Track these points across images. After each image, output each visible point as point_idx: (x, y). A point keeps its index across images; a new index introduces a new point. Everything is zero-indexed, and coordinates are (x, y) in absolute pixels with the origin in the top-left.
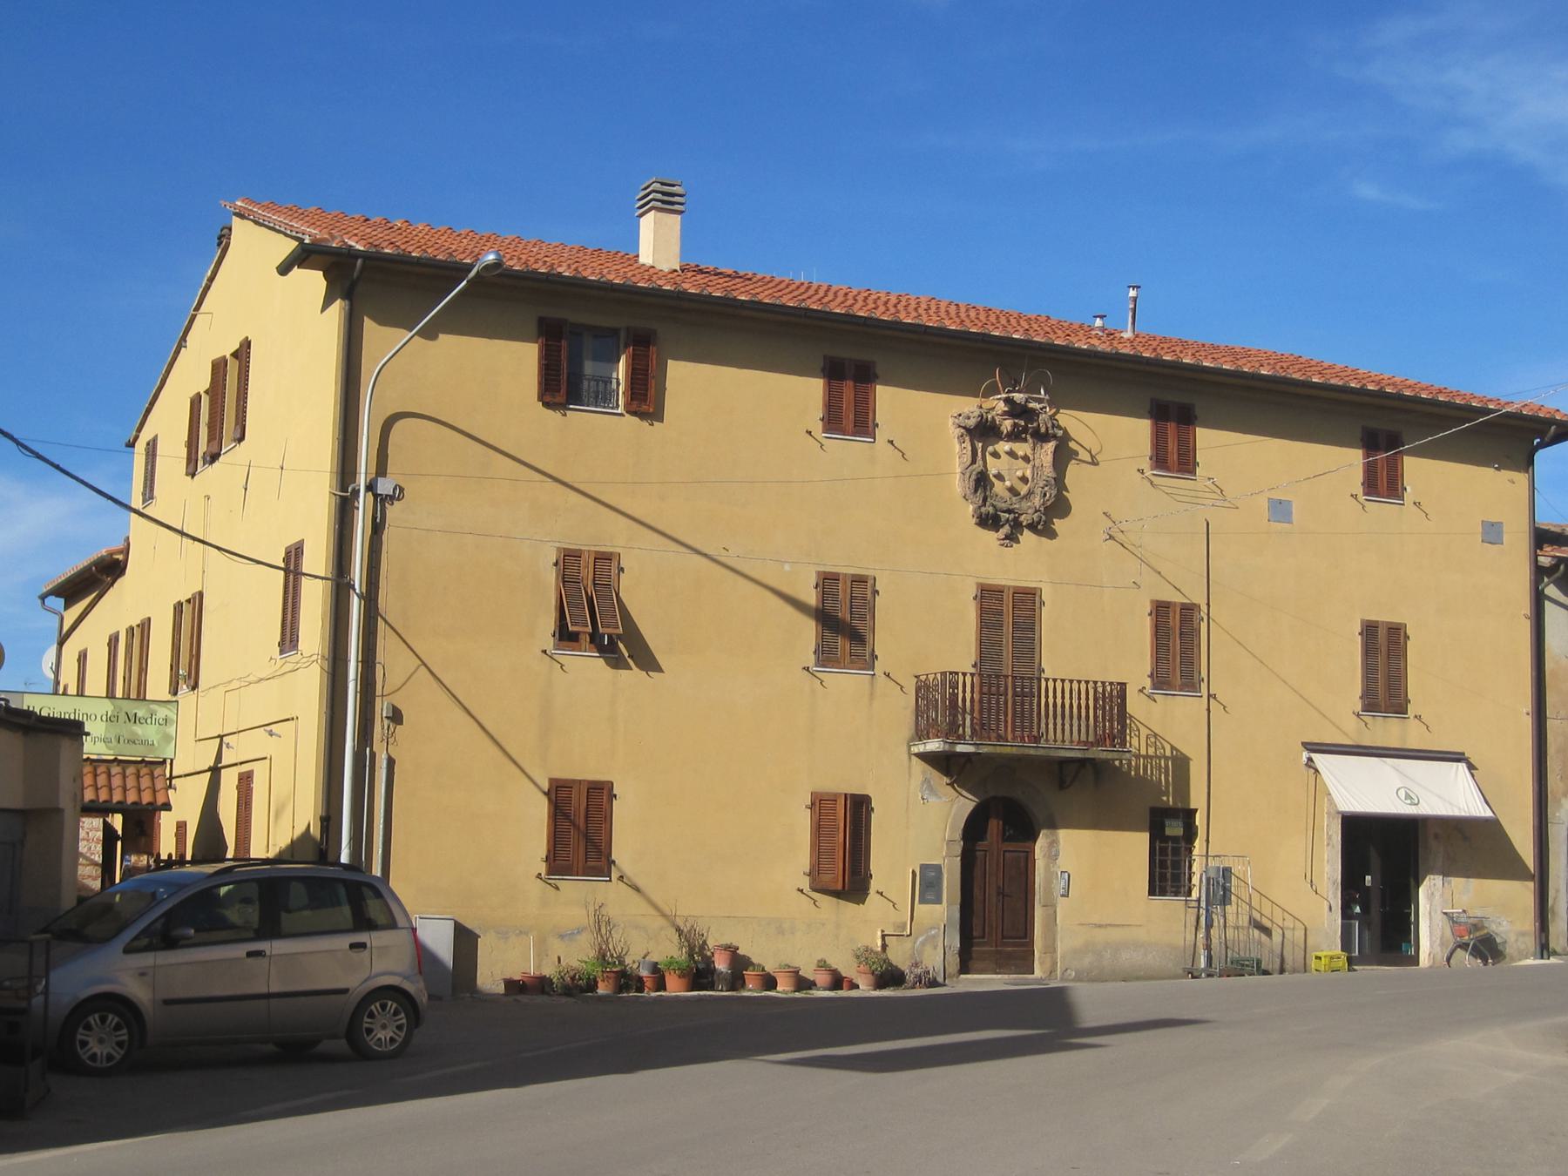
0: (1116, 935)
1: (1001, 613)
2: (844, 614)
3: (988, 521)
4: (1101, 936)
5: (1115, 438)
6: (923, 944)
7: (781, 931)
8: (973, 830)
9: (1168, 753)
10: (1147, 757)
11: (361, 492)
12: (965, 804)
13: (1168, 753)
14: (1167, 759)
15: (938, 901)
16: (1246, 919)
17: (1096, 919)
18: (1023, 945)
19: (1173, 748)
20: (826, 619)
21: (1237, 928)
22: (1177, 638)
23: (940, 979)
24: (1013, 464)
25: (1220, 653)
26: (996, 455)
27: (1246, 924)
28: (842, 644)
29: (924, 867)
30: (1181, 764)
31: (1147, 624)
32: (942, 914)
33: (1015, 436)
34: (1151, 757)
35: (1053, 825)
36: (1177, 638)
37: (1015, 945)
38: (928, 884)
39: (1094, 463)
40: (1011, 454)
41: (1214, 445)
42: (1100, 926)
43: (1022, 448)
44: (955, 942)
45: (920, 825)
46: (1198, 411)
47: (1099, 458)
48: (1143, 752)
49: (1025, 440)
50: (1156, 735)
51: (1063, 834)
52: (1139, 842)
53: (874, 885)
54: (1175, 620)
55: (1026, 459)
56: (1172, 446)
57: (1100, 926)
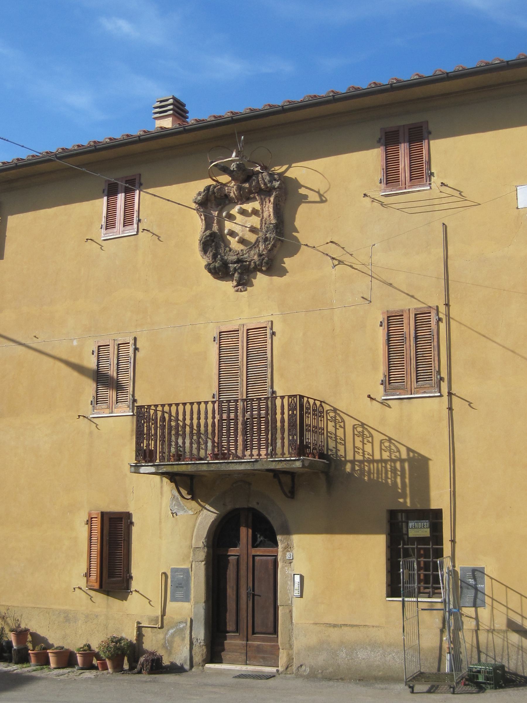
0: (350, 635)
1: (236, 349)
2: (112, 372)
3: (220, 271)
4: (335, 634)
5: (340, 181)
6: (173, 635)
7: (67, 619)
8: (220, 540)
9: (404, 456)
10: (382, 461)
11: (522, 656)
12: (208, 516)
13: (404, 456)
14: (402, 461)
15: (186, 599)
16: (504, 622)
17: (330, 619)
18: (271, 640)
19: (409, 450)
20: (100, 378)
21: (491, 631)
22: (414, 351)
23: (187, 667)
24: (244, 223)
25: (465, 356)
26: (231, 217)
27: (504, 627)
28: (112, 394)
29: (174, 571)
30: (419, 465)
31: (381, 334)
32: (190, 609)
33: (245, 197)
34: (386, 461)
35: (287, 532)
36: (414, 351)
37: (263, 640)
38: (175, 585)
39: (323, 200)
40: (243, 212)
41: (446, 152)
42: (335, 626)
43: (249, 207)
44: (200, 633)
45: (170, 534)
46: (431, 127)
47: (327, 196)
48: (377, 457)
49: (254, 199)
50: (390, 440)
51: (296, 538)
52: (373, 548)
53: (134, 585)
54: (409, 327)
55: (255, 212)
56: (404, 163)
57: (335, 626)
